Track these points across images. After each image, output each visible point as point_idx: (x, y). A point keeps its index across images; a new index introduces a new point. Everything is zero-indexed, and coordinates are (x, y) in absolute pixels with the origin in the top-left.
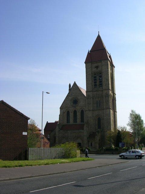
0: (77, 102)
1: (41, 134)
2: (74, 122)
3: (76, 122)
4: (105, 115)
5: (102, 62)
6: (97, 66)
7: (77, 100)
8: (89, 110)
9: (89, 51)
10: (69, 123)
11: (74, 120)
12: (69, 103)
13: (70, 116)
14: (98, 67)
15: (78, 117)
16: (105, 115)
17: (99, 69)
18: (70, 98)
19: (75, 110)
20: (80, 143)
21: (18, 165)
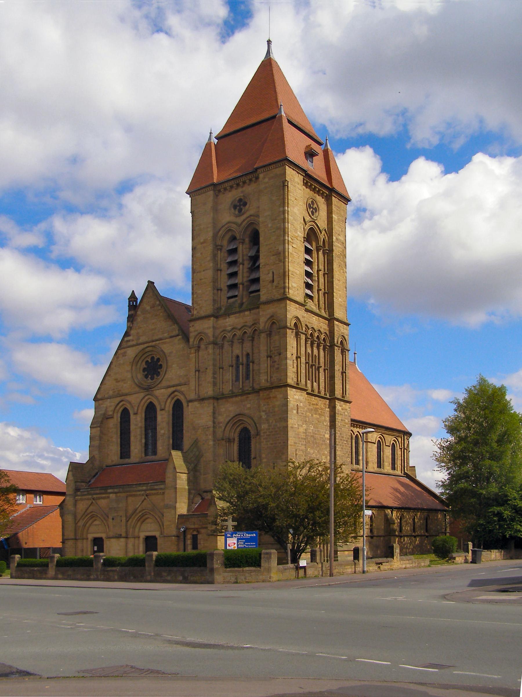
0: (161, 366)
1: (273, 524)
2: (146, 454)
3: (155, 453)
4: (264, 416)
5: (261, 176)
6: (240, 200)
7: (158, 360)
8: (202, 400)
9: (214, 135)
10: (366, 510)
11: (146, 444)
12: (129, 375)
13: (132, 427)
14: (245, 204)
15: (162, 432)
16: (263, 414)
17: (250, 210)
18: (131, 353)
19: (151, 403)
20: (154, 538)
21: (95, 614)
